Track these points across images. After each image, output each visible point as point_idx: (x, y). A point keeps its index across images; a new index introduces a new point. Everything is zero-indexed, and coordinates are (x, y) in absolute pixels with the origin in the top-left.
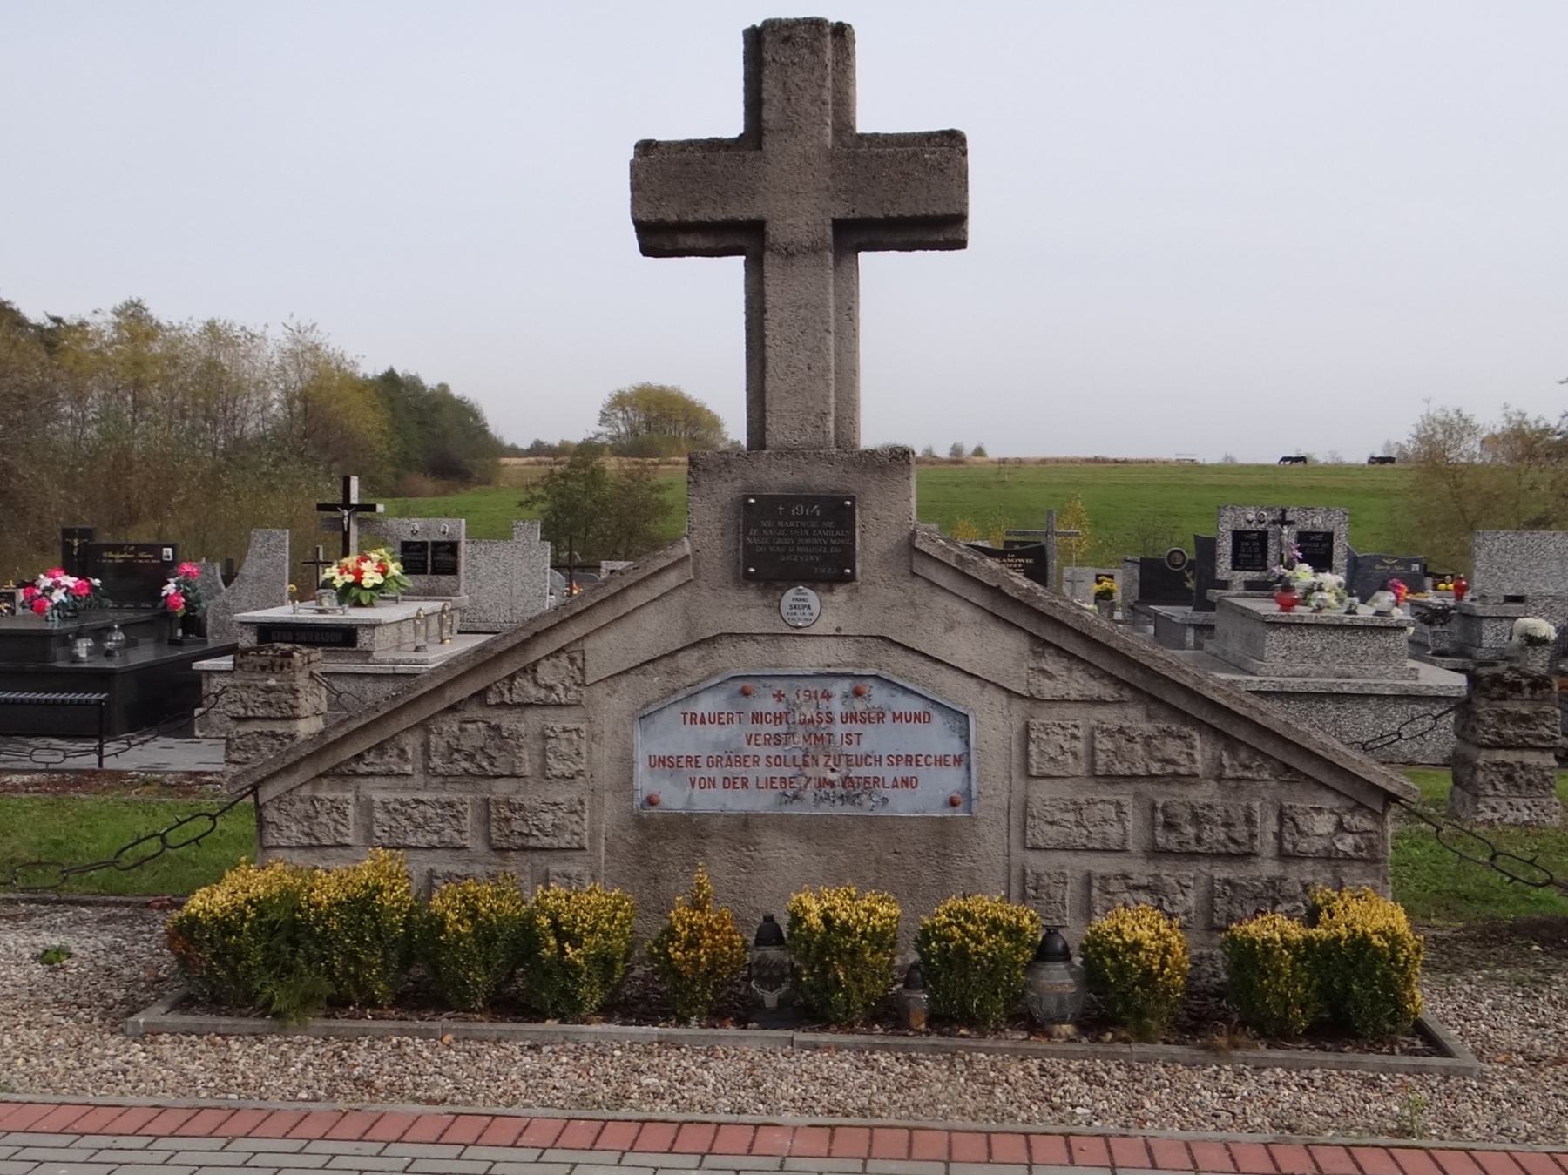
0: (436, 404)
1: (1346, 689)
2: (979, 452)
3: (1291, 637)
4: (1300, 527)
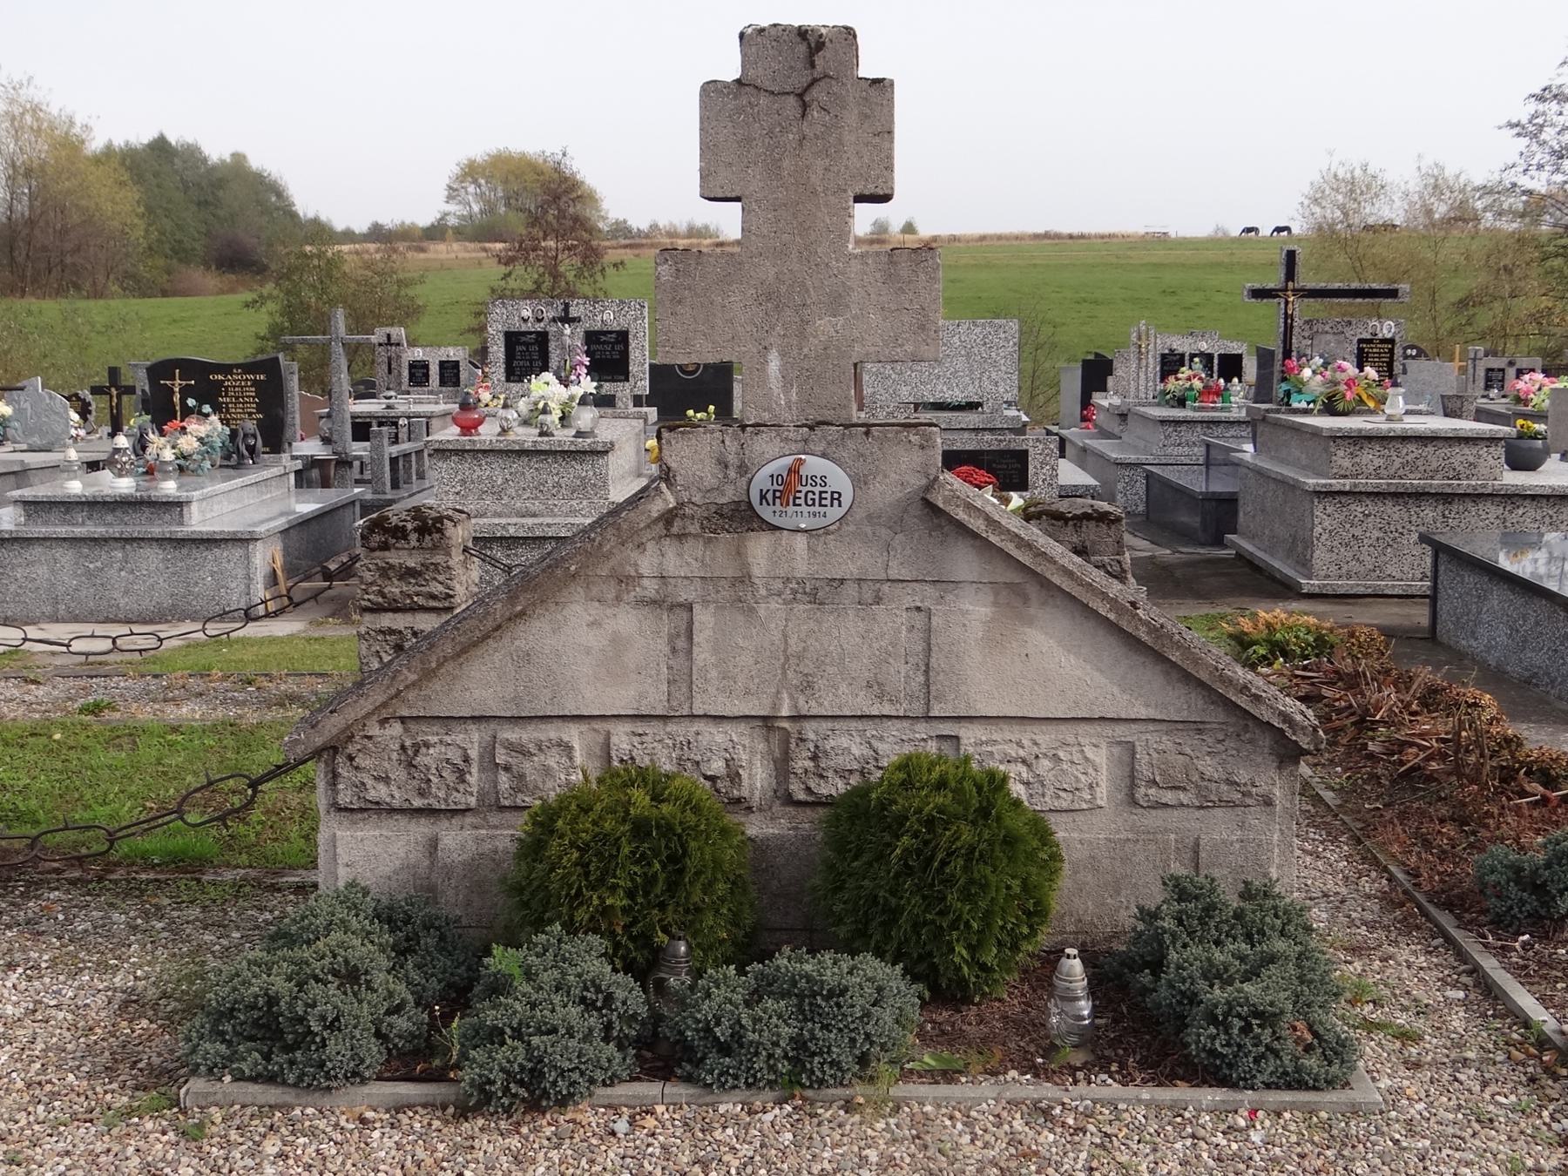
0: (220, 180)
1: (512, 531)
2: (909, 228)
3: (466, 467)
4: (587, 325)
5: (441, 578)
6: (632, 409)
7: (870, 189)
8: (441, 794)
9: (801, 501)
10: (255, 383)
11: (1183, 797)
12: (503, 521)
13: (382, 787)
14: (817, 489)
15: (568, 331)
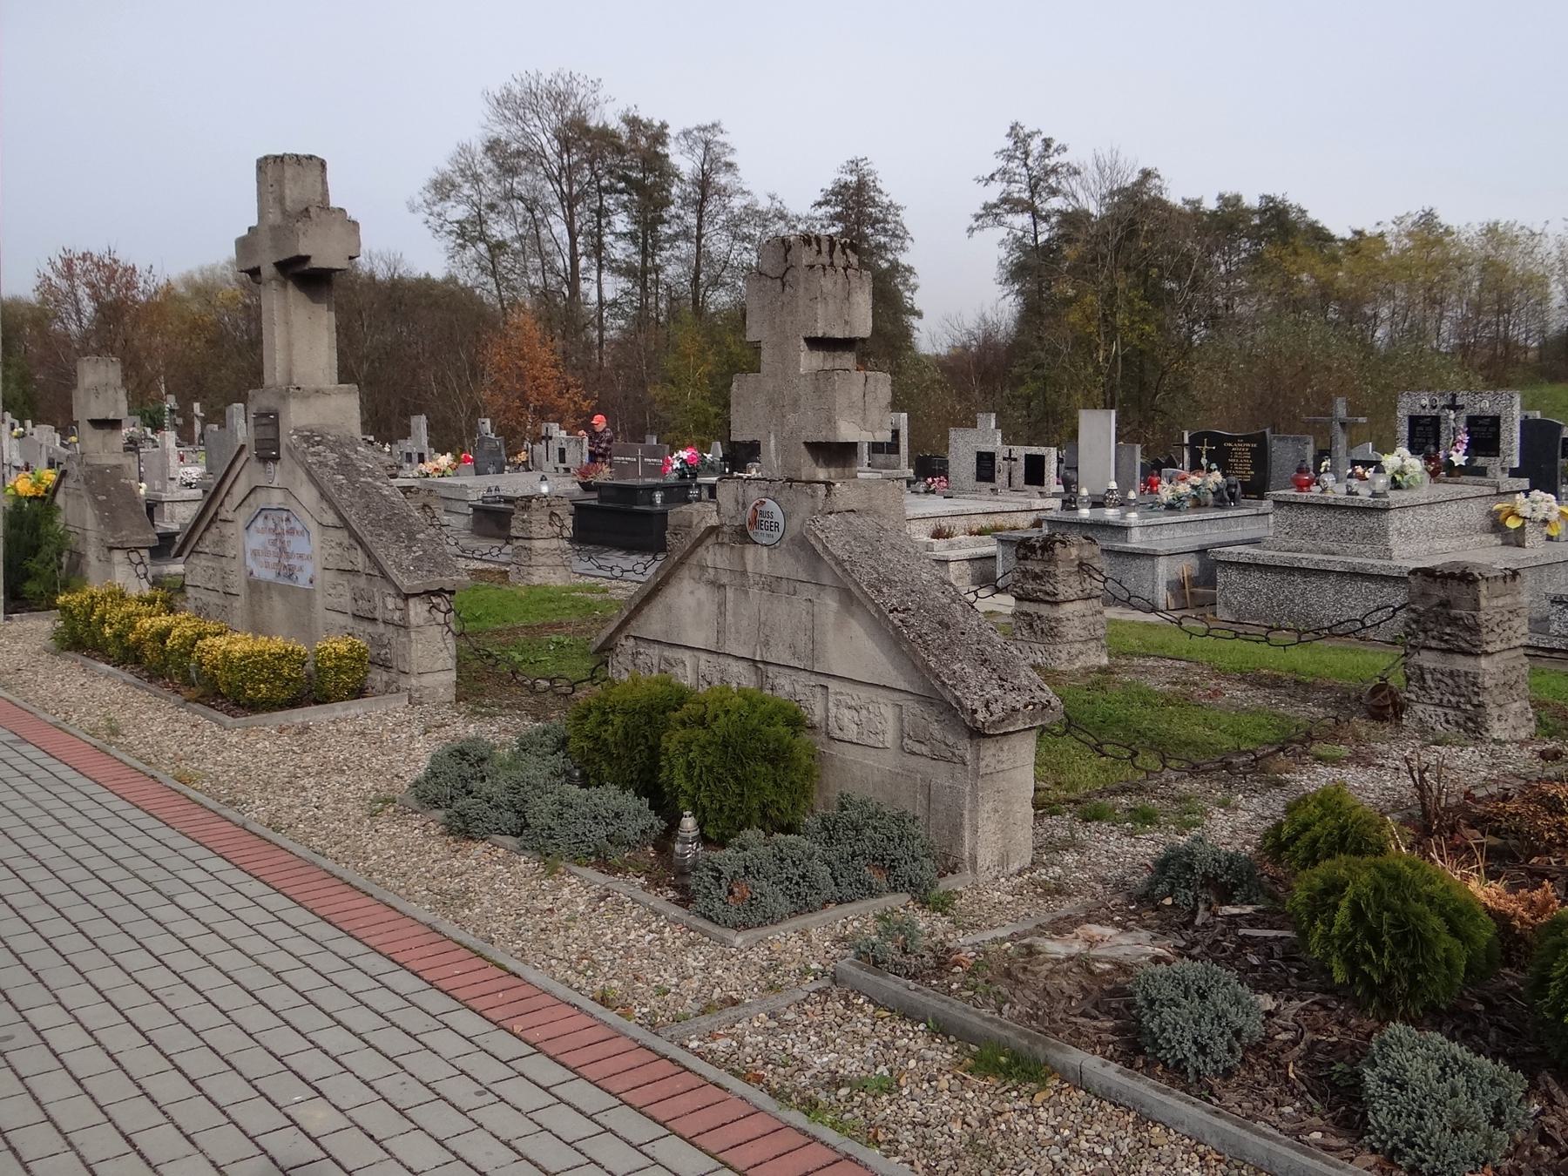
11: (924, 749)
12: (1300, 556)
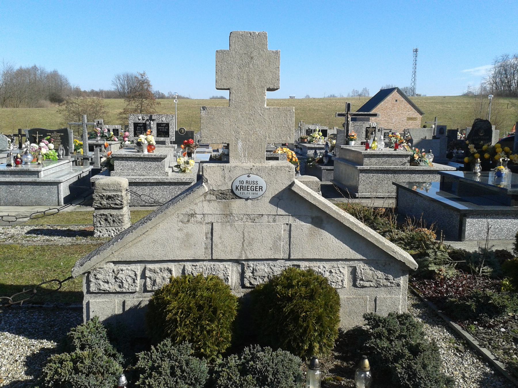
1: (137, 180)
4: (157, 121)
5: (119, 199)
6: (170, 145)
7: (272, 87)
8: (127, 287)
9: (250, 189)
10: (60, 136)
13: (106, 285)
14: (255, 186)
15: (152, 123)
